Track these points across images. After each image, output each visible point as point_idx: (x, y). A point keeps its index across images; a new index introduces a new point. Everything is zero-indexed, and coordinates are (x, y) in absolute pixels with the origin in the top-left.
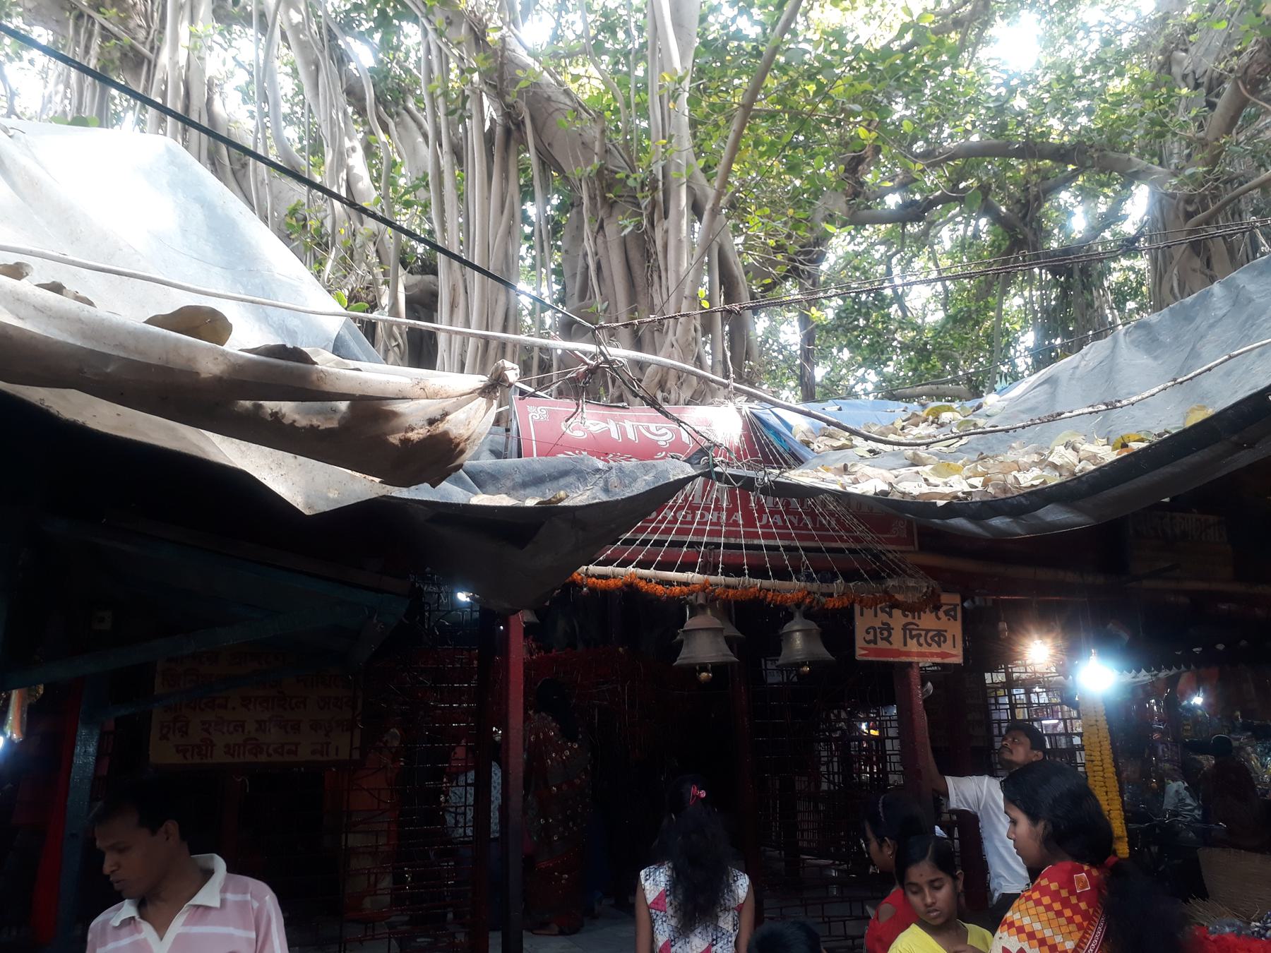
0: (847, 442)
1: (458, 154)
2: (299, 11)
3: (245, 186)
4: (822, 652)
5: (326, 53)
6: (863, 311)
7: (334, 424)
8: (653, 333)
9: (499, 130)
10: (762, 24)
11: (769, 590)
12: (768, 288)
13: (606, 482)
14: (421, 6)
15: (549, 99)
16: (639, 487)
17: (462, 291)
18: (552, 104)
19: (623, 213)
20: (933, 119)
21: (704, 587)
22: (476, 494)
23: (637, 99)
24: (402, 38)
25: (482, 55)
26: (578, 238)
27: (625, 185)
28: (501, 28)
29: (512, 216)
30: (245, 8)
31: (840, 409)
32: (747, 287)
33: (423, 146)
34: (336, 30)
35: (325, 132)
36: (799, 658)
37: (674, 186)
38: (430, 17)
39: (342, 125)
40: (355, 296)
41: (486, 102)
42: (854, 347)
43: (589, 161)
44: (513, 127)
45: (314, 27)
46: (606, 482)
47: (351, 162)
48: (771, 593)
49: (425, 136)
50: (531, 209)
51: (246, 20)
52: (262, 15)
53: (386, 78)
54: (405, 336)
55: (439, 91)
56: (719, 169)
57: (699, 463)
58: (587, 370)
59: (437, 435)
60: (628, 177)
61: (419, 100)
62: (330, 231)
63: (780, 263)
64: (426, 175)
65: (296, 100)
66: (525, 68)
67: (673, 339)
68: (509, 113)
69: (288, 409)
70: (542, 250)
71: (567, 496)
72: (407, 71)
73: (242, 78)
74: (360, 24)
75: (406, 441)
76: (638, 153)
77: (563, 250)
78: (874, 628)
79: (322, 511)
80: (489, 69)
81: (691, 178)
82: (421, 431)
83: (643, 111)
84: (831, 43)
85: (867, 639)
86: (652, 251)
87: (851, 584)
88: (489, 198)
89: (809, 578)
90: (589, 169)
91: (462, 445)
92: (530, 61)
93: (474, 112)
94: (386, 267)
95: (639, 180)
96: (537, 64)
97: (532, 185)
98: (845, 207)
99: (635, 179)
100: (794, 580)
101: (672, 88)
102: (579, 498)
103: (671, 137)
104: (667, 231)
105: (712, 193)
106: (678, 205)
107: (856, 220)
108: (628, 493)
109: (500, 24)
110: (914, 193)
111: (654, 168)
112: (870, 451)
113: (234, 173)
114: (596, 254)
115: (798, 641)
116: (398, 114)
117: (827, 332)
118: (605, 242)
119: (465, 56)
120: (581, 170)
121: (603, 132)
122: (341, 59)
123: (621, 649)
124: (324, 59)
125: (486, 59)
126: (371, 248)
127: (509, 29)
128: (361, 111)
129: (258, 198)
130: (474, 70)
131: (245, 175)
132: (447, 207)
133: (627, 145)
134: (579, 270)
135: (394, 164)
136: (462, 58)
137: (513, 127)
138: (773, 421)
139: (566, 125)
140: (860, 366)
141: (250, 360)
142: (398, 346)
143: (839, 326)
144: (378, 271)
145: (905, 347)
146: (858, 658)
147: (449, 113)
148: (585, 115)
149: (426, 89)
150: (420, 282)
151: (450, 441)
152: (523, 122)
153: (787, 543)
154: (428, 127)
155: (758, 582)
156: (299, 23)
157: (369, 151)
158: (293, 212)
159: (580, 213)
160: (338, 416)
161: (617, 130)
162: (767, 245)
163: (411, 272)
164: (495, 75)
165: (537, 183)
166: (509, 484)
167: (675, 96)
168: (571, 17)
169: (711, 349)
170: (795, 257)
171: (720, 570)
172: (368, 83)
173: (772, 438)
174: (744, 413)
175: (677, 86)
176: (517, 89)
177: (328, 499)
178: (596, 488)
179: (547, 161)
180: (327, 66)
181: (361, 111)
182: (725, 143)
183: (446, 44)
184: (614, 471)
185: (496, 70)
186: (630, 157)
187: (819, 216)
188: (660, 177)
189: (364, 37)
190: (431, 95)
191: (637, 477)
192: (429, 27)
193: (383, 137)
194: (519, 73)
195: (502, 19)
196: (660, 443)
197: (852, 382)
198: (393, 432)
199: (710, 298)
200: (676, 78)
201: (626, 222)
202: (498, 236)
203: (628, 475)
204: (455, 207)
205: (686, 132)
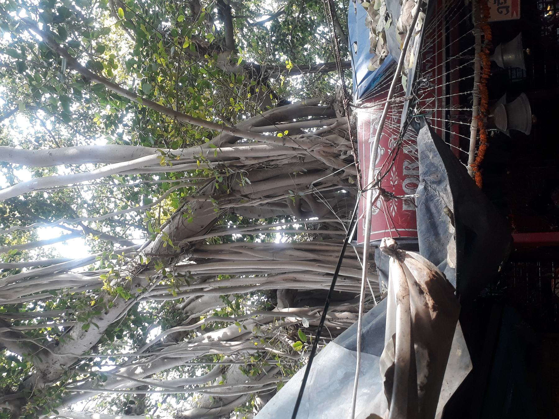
0: (381, 35)
1: (205, 279)
2: (136, 368)
3: (232, 399)
4: (518, 39)
5: (158, 353)
6: (282, 38)
7: (426, 352)
8: (305, 163)
9: (195, 256)
10: (127, 109)
11: (481, 77)
12: (275, 96)
13: (434, 182)
14: (131, 301)
15: (177, 228)
16: (438, 161)
17: (286, 276)
18: (180, 226)
19: (237, 184)
20: (172, 5)
21: (479, 119)
22: (446, 264)
23: (174, 178)
24: (145, 311)
25: (156, 266)
26: (251, 210)
27: (222, 183)
28: (140, 256)
29: (242, 247)
30: (135, 398)
31: (356, 43)
32: (274, 110)
33: (203, 298)
34: (145, 348)
35: (200, 354)
36: (521, 56)
37: (222, 155)
38: (136, 295)
39: (196, 344)
40: (292, 337)
41: (180, 263)
42: (303, 41)
43: (210, 204)
44: (194, 248)
45: (144, 360)
46: (434, 182)
47: (216, 339)
48: (482, 75)
49: (198, 297)
50: (236, 236)
51: (142, 398)
52: (138, 388)
53: (167, 320)
54: (312, 308)
55: (176, 290)
56: (211, 129)
57: (419, 124)
58: (382, 195)
59: (429, 289)
60: (217, 182)
61: (178, 301)
62: (256, 351)
63: (261, 89)
64: (221, 296)
65: (181, 370)
66: (161, 243)
67: (308, 150)
68: (185, 251)
69: (420, 379)
70: (258, 230)
71: (446, 207)
72: (163, 308)
73: (172, 400)
74: (139, 335)
75: (434, 308)
76: (203, 177)
77: (258, 218)
78: (498, 9)
79: (470, 359)
80: (163, 262)
81: (217, 146)
82: (427, 298)
83: (179, 174)
84: (133, 68)
85: (506, 13)
86: (258, 166)
87: (475, 24)
88: (233, 261)
89: (472, 53)
90: (214, 204)
91: (434, 273)
92: (157, 239)
93: (187, 270)
94: (275, 318)
95: (219, 175)
96: (159, 235)
97: (223, 237)
98: (225, 54)
99: (218, 177)
100: (474, 61)
101: (168, 158)
102: (445, 199)
103: (195, 158)
104: (247, 158)
105: (224, 132)
106: (231, 152)
107: (233, 48)
108: (442, 167)
109: (138, 257)
110: (214, 13)
111: (212, 167)
112: (386, 20)
113: (225, 405)
114: (261, 198)
115: (510, 57)
116: (186, 313)
117: (296, 59)
118: (254, 193)
119: (157, 276)
120: (215, 209)
121: (193, 197)
122: (158, 346)
123: (508, 173)
124: (160, 355)
125: (158, 264)
126: (264, 327)
127: (140, 251)
128: (186, 334)
129: (240, 392)
130: (164, 271)
131: (226, 399)
132: (238, 285)
133: (197, 183)
134: (270, 208)
135: (216, 314)
136: (158, 278)
137: (194, 248)
138: (365, 84)
139: (191, 218)
140: (315, 37)
141: (395, 404)
142: (319, 312)
143: (292, 52)
144: (277, 324)
145: (303, 11)
146: (519, 17)
147: (189, 284)
148: (185, 208)
149: (175, 297)
150: (281, 299)
151: (431, 280)
152: (190, 242)
153: (444, 69)
154: (192, 296)
155: (475, 84)
156: (142, 368)
157: (208, 329)
158: (246, 372)
159: (237, 209)
160: (421, 349)
161: (190, 189)
162: (250, 97)
163: (276, 304)
164: (166, 259)
165: (220, 234)
166: (436, 244)
167: (173, 157)
168: (128, 218)
169: (307, 128)
170: (257, 80)
171: (468, 109)
172: (170, 331)
173: (376, 83)
174: (361, 103)
175: (167, 155)
176: (173, 246)
177: (462, 356)
178: (438, 189)
179: (211, 228)
180: (166, 353)
181: (186, 334)
182: (196, 126)
183: (151, 286)
184: (426, 178)
185: (163, 258)
186: (207, 181)
187: (231, 69)
188: (217, 163)
189: (146, 331)
190: (179, 294)
191: (431, 162)
192: (142, 297)
193: (202, 321)
194: (165, 245)
195: (135, 256)
196: (382, 154)
197: (324, 41)
198: (429, 316)
199: (282, 131)
200: (163, 157)
201: (243, 181)
202: (254, 255)
203: (429, 169)
204: (238, 280)
205: (191, 150)
